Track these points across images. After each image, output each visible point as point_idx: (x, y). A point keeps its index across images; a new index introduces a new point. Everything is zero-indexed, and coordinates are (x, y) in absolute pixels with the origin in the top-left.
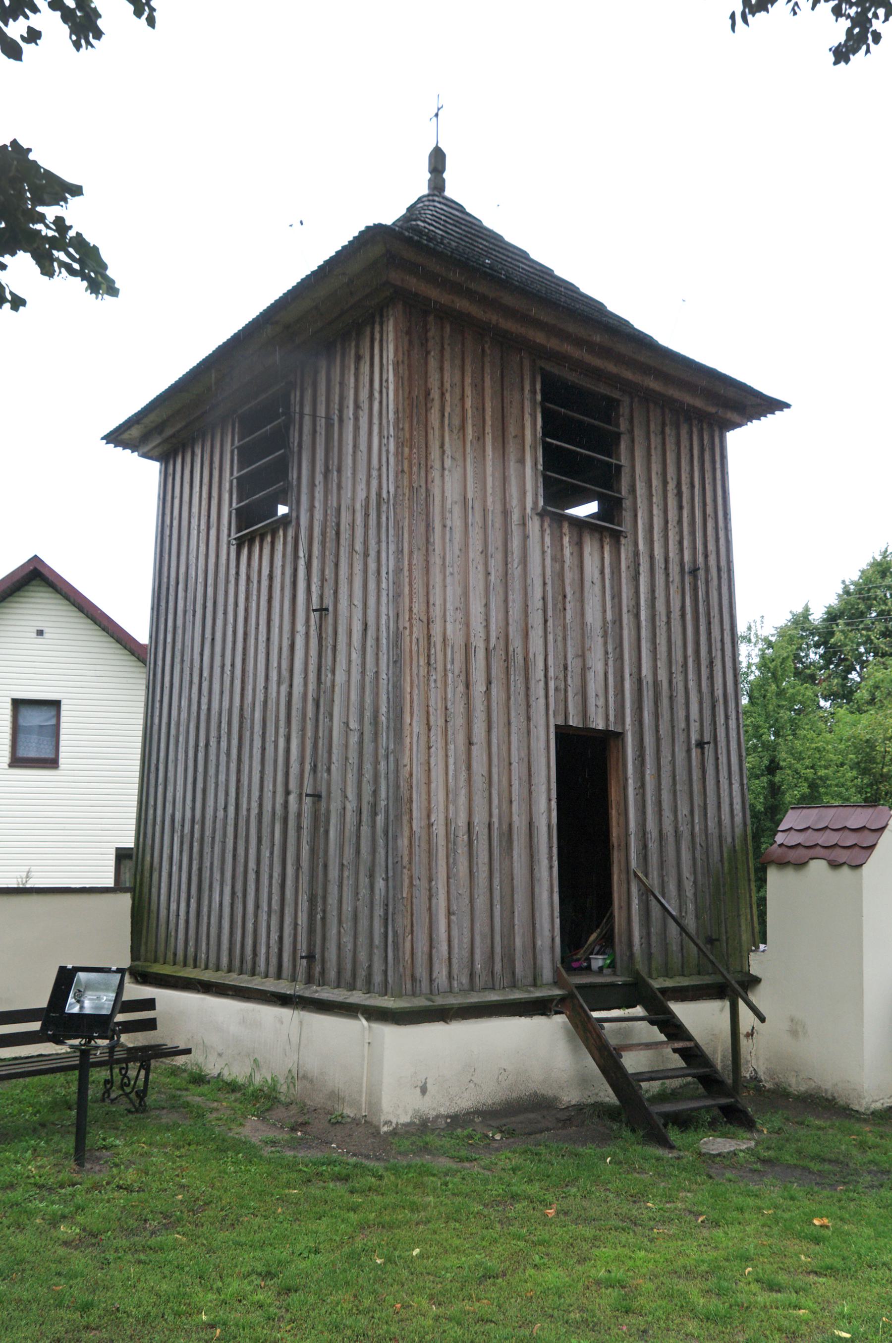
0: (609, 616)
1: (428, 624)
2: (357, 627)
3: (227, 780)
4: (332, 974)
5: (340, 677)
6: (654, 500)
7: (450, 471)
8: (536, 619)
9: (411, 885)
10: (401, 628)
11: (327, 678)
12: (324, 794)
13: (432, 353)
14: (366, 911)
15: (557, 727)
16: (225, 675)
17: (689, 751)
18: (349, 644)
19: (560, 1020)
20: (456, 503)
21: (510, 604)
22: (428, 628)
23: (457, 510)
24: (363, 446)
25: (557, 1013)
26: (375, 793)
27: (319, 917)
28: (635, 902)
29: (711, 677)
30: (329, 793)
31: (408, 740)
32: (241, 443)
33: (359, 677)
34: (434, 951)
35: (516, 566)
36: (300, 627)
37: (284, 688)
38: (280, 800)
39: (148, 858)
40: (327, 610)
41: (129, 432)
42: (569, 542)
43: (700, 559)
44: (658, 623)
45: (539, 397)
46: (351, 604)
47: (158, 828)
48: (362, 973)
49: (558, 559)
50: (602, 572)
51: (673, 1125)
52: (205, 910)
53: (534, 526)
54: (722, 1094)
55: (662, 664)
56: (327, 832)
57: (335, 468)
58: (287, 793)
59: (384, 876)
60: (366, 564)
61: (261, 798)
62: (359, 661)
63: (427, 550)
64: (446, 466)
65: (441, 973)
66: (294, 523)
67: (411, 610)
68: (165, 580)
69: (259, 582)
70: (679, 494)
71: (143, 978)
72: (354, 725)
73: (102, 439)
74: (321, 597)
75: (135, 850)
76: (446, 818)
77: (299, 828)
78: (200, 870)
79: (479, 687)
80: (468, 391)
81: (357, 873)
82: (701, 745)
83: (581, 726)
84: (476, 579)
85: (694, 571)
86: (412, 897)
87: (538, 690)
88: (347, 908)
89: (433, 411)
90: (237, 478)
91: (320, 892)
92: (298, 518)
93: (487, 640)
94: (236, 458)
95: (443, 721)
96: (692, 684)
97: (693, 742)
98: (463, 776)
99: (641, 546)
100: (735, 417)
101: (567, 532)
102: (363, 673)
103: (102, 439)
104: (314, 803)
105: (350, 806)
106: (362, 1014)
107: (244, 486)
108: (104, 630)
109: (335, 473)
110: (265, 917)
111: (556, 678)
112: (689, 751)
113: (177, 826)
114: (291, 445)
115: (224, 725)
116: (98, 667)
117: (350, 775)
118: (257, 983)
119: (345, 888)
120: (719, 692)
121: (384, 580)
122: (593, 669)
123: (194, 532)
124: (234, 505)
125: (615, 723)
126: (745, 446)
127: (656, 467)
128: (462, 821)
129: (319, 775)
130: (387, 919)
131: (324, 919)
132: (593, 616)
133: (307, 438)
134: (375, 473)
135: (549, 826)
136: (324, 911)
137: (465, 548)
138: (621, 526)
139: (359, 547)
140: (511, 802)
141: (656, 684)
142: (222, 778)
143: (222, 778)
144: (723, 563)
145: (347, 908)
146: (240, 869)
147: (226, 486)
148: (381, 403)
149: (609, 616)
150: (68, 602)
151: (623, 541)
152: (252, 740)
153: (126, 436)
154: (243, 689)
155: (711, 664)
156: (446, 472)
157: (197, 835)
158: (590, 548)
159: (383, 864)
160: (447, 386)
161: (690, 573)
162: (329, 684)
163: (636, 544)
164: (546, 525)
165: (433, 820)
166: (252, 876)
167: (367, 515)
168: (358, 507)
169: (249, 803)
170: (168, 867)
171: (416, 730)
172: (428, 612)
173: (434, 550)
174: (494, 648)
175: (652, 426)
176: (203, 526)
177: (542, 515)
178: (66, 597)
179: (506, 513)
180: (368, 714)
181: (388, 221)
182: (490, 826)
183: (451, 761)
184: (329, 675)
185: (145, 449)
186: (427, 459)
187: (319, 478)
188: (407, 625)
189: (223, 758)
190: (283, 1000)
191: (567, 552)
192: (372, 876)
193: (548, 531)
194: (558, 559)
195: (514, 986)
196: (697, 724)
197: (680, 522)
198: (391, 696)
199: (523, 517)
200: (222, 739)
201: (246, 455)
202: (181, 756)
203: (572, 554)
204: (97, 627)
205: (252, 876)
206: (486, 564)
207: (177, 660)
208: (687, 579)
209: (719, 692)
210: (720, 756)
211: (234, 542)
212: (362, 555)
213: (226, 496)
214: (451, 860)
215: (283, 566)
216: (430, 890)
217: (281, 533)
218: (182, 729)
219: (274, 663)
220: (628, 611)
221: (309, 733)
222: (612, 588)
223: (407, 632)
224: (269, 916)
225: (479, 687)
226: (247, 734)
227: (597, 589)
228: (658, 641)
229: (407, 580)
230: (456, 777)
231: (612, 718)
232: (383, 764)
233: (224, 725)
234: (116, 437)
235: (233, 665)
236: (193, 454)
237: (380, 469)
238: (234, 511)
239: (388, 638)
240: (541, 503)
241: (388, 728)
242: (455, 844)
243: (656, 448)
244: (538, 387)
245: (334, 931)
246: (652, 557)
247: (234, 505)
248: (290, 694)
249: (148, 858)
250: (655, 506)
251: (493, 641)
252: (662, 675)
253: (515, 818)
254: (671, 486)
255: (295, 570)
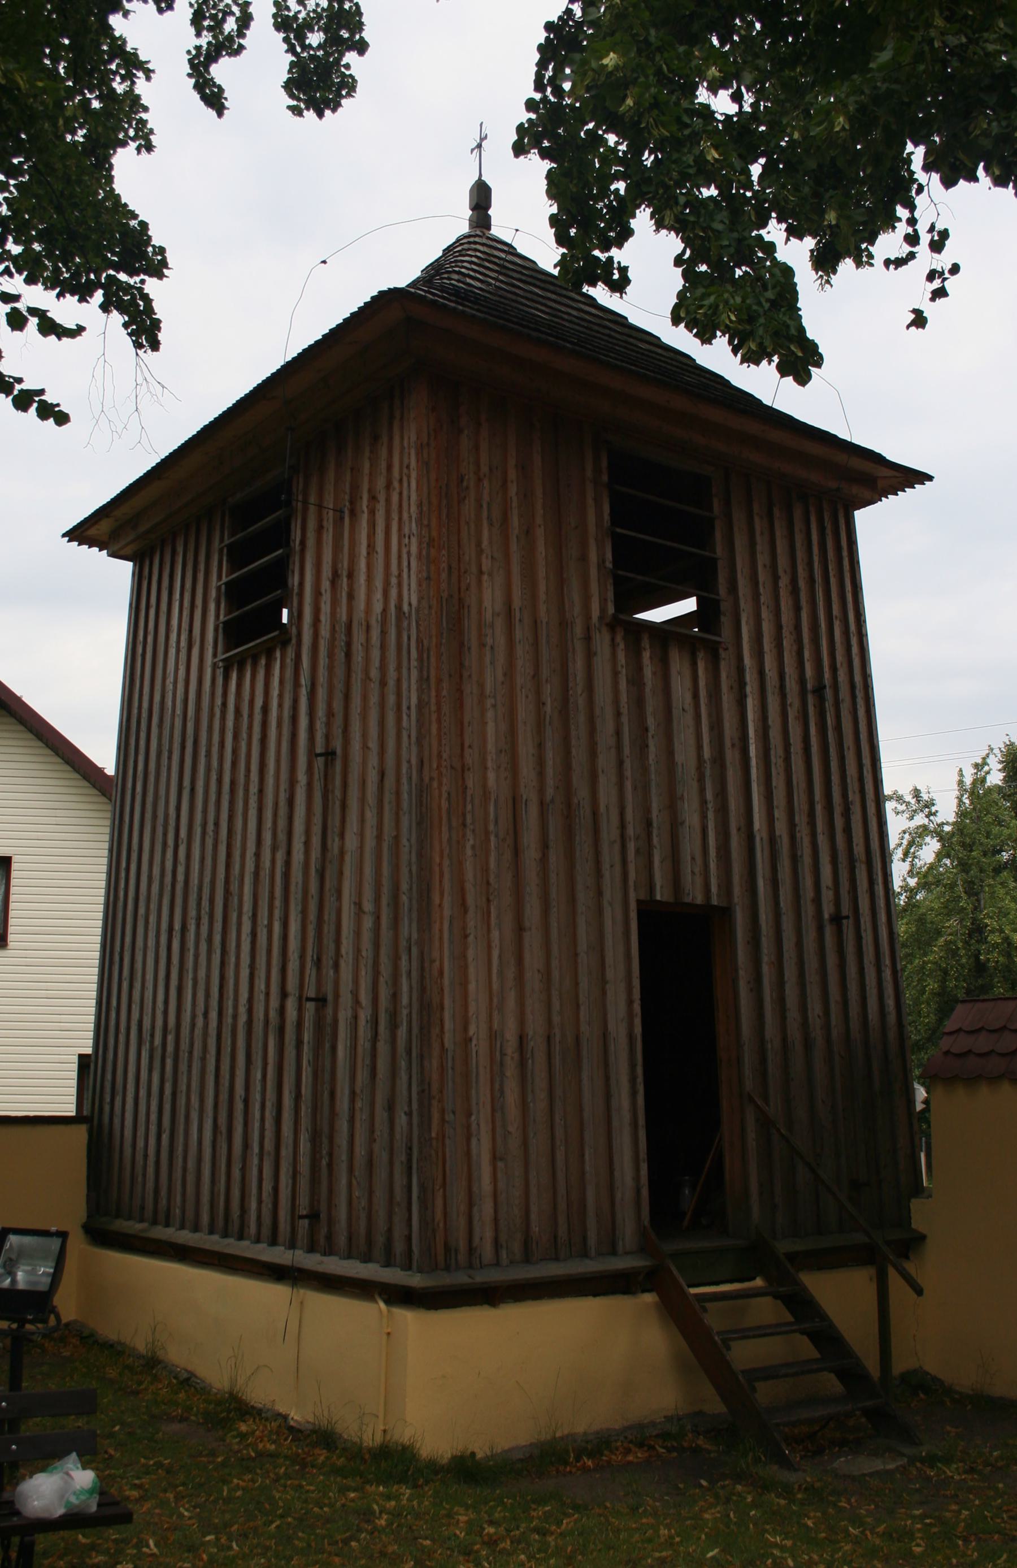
0: (707, 754)
1: (463, 771)
2: (373, 776)
3: (208, 977)
4: (342, 1240)
5: (351, 842)
6: (762, 599)
7: (490, 575)
8: (606, 761)
9: (443, 1121)
10: (427, 779)
11: (334, 845)
12: (330, 998)
13: (466, 432)
14: (385, 1156)
15: (639, 902)
16: (207, 838)
17: (820, 929)
18: (363, 800)
19: (649, 1298)
20: (498, 615)
21: (573, 742)
22: (463, 779)
23: (500, 623)
24: (380, 547)
25: (644, 1291)
26: (395, 996)
27: (324, 1162)
28: (751, 1135)
29: (848, 830)
30: (337, 996)
31: (436, 927)
32: (233, 539)
33: (374, 843)
34: (475, 1209)
35: (579, 692)
36: (302, 777)
37: (280, 856)
38: (274, 1003)
39: (109, 1076)
40: (333, 753)
41: (97, 526)
42: (651, 658)
43: (827, 675)
44: (773, 759)
45: (605, 478)
46: (365, 747)
47: (122, 1038)
48: (380, 1239)
49: (636, 681)
50: (696, 696)
51: (907, 1257)
52: (180, 1149)
53: (602, 641)
54: (880, 1406)
55: (780, 814)
56: (334, 1048)
57: (345, 573)
58: (284, 995)
59: (406, 1109)
60: (383, 697)
61: (250, 1000)
62: (374, 822)
63: (461, 676)
64: (484, 568)
65: (484, 1235)
66: (294, 641)
67: (440, 756)
68: (135, 711)
69: (251, 716)
70: (795, 591)
71: (100, 1235)
72: (368, 906)
73: (64, 535)
74: (327, 737)
75: (93, 1058)
76: (490, 1028)
77: (299, 1043)
78: (174, 1094)
79: (531, 854)
80: (512, 474)
81: (372, 1104)
82: (837, 919)
83: (672, 900)
84: (524, 710)
85: (819, 690)
86: (444, 1137)
87: (610, 856)
88: (360, 1151)
89: (467, 501)
90: (226, 584)
91: (326, 1129)
92: (299, 635)
93: (541, 790)
94: (225, 563)
95: (484, 899)
96: (822, 840)
97: (826, 916)
98: (511, 973)
99: (747, 661)
100: (867, 494)
101: (648, 646)
102: (379, 838)
103: (64, 535)
104: (317, 1010)
105: (364, 1016)
106: (380, 1295)
107: (235, 593)
108: (67, 763)
109: (345, 580)
110: (256, 1161)
111: (637, 838)
112: (820, 929)
113: (146, 1036)
114: (292, 544)
115: (205, 903)
116: (59, 813)
117: (363, 973)
118: (246, 1249)
119: (358, 1124)
120: (859, 849)
121: (405, 717)
122: (687, 824)
123: (172, 651)
124: (222, 618)
125: (719, 896)
126: (878, 528)
127: (763, 559)
128: (511, 1036)
129: (324, 971)
130: (410, 1168)
131: (330, 1165)
132: (685, 755)
133: (311, 536)
134: (394, 581)
135: (631, 1037)
136: (331, 1155)
137: (510, 673)
138: (720, 636)
139: (374, 673)
140: (578, 1006)
141: (772, 839)
142: (202, 973)
143: (202, 973)
144: (858, 678)
145: (360, 1151)
146: (224, 1097)
147: (213, 593)
148: (401, 494)
149: (707, 754)
150: (22, 728)
151: (723, 654)
152: (239, 924)
153: (92, 532)
154: (229, 855)
155: (847, 813)
156: (485, 577)
157: (170, 1048)
158: (678, 663)
159: (405, 1093)
160: (484, 469)
161: (814, 692)
162: (336, 851)
163: (740, 658)
164: (619, 638)
165: (471, 1033)
166: (239, 1106)
167: (384, 633)
168: (373, 622)
169: (236, 1007)
170: (133, 1090)
171: (447, 912)
172: (462, 756)
173: (470, 676)
174: (552, 801)
175: (756, 508)
176: (183, 643)
177: (612, 627)
178: (22, 721)
179: (564, 625)
180: (386, 890)
181: (402, 283)
182: (549, 1039)
183: (495, 953)
184: (337, 839)
185: (116, 547)
186: (459, 561)
187: (326, 585)
188: (435, 774)
189: (203, 947)
190: (278, 1273)
191: (648, 671)
192: (391, 1107)
193: (622, 646)
194: (636, 681)
195: (585, 1254)
196: (831, 893)
197: (798, 627)
198: (414, 868)
199: (588, 629)
200: (202, 921)
201: (237, 555)
202: (151, 943)
203: (654, 673)
204: (59, 760)
205: (239, 1106)
206: (538, 692)
207: (148, 815)
208: (811, 700)
209: (859, 849)
210: (863, 935)
211: (221, 664)
212: (377, 683)
213: (212, 607)
214: (497, 1086)
215: (281, 696)
216: (468, 1127)
217: (278, 654)
218: (153, 906)
219: (268, 824)
220: (733, 745)
221: (312, 916)
222: (710, 715)
223: (435, 784)
224: (261, 1160)
225: (531, 854)
226: (234, 917)
227: (689, 719)
228: (774, 784)
229: (434, 717)
230: (501, 973)
231: (714, 889)
232: (404, 958)
233: (205, 903)
234: (79, 534)
235: (217, 824)
236: (174, 553)
237: (400, 576)
238: (221, 625)
239: (410, 793)
240: (611, 610)
241: (410, 910)
242: (502, 1064)
243: (762, 533)
244: (604, 464)
245: (344, 1181)
246: (761, 673)
247: (222, 618)
248: (288, 863)
249: (109, 1076)
250: (764, 609)
251: (550, 792)
252: (781, 828)
253: (584, 1028)
254: (784, 582)
255: (295, 702)
